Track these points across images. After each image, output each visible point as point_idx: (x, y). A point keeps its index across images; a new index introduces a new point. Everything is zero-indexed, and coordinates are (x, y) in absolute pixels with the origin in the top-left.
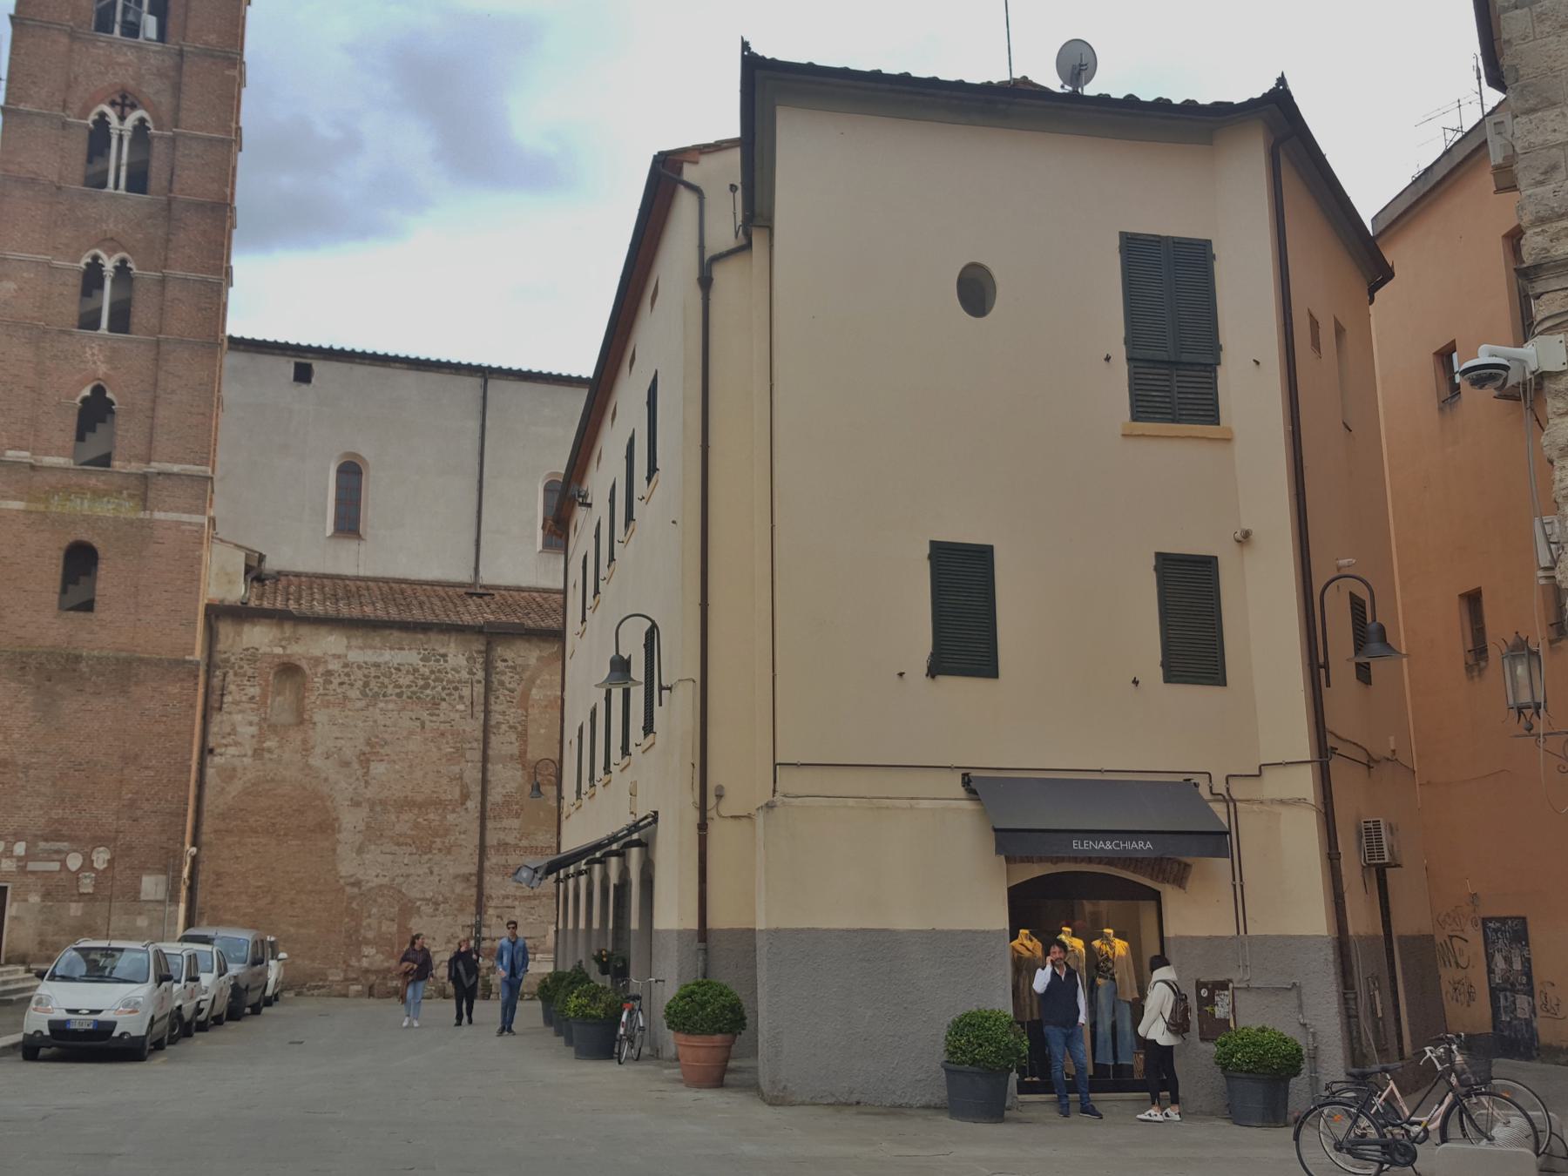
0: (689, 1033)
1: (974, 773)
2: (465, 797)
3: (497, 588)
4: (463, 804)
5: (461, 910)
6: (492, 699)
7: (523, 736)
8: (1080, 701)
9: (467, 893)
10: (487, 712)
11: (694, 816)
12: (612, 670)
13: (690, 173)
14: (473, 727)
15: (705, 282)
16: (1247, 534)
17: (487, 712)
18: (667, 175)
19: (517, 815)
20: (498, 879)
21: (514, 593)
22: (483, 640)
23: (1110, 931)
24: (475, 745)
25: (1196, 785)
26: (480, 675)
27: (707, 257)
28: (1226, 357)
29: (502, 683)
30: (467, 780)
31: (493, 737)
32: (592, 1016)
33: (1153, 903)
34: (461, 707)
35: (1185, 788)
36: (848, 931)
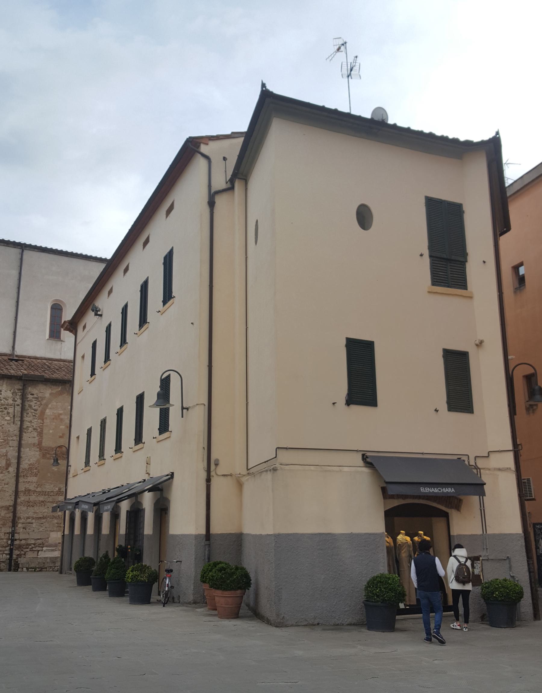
0: (225, 590)
1: (368, 454)
2: (8, 465)
3: (25, 357)
4: (7, 469)
5: (4, 525)
6: (25, 414)
7: (40, 434)
8: (411, 421)
9: (8, 515)
10: (22, 421)
11: (204, 475)
12: (158, 399)
13: (204, 149)
14: (14, 429)
15: (211, 204)
16: (481, 342)
17: (22, 421)
18: (191, 149)
19: (36, 475)
20: (25, 508)
21: (34, 360)
22: (21, 383)
23: (422, 532)
24: (15, 438)
25: (464, 461)
26: (19, 401)
27: (212, 191)
28: (470, 258)
29: (30, 406)
30: (9, 456)
31: (24, 434)
32: (142, 581)
33: (445, 519)
34: (8, 418)
35: (458, 463)
36: (312, 534)
